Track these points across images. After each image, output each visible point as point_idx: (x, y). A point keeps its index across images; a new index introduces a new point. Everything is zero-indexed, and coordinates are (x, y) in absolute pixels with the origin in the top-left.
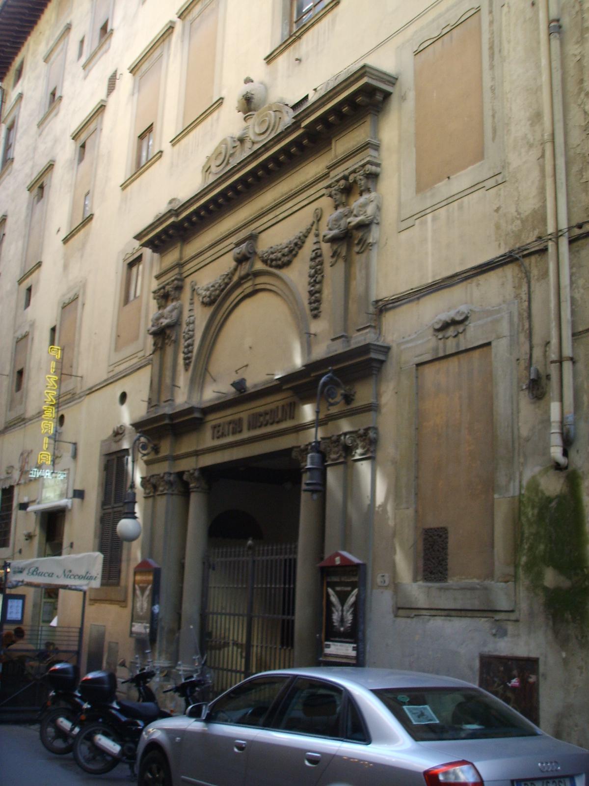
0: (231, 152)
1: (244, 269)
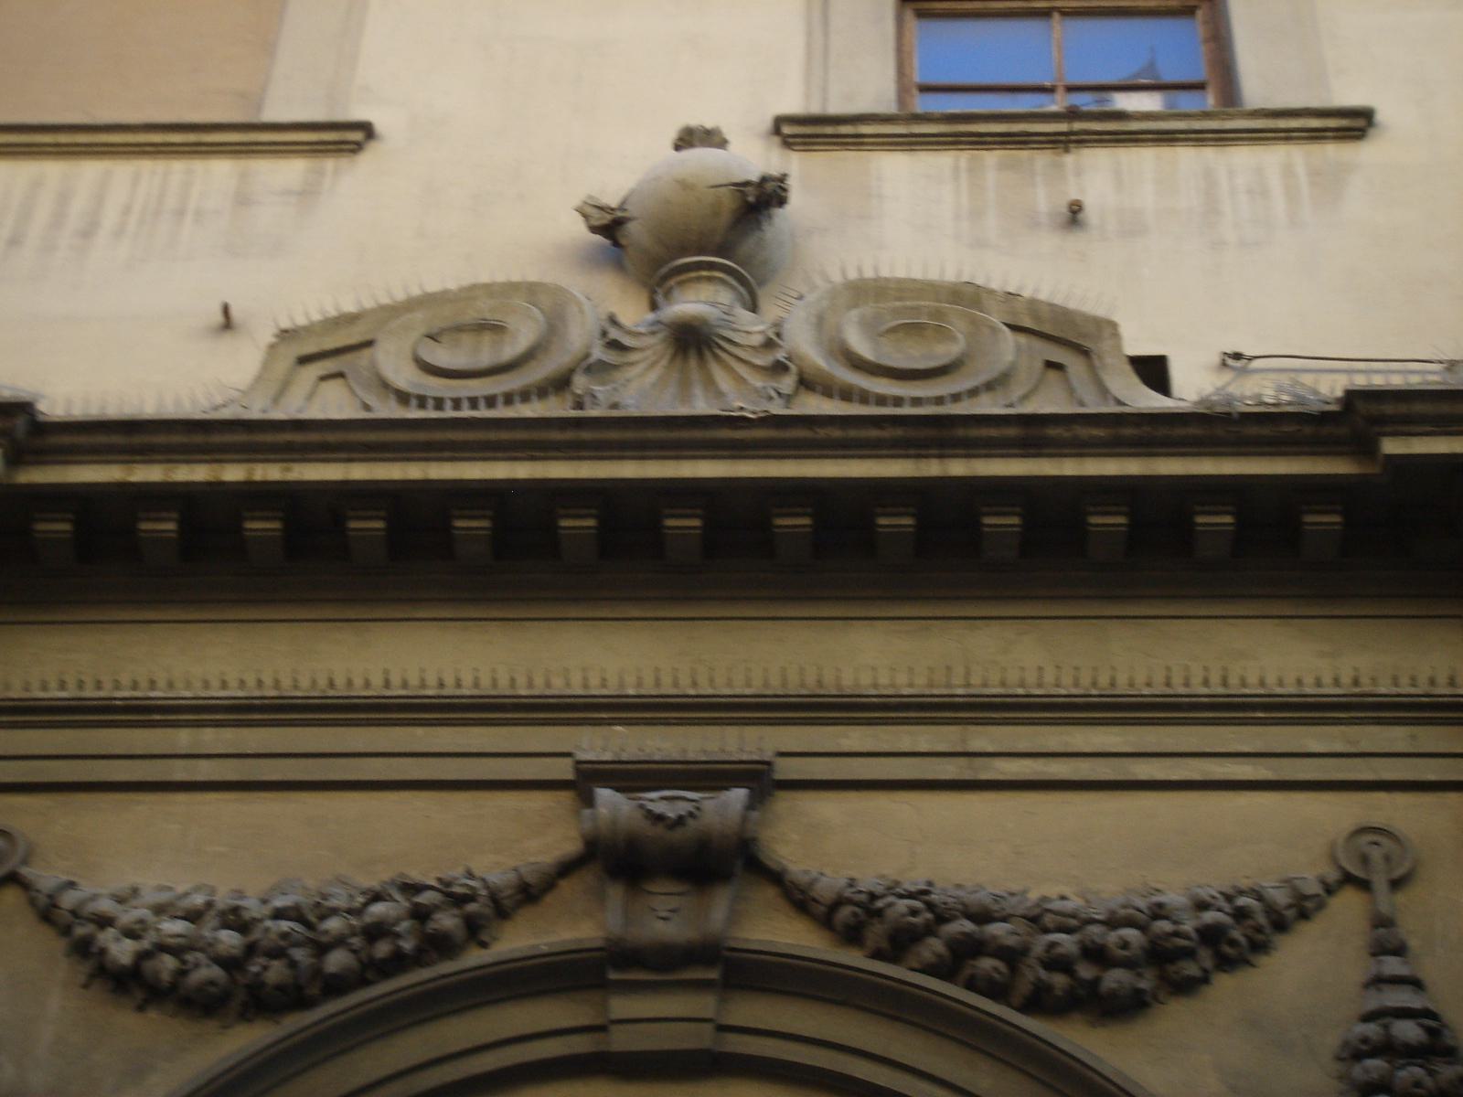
0: (598, 353)
1: (666, 917)
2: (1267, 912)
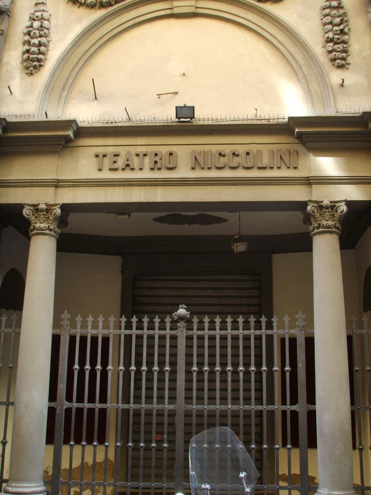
2: (236, 451)
